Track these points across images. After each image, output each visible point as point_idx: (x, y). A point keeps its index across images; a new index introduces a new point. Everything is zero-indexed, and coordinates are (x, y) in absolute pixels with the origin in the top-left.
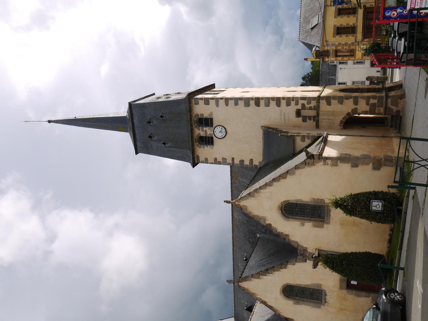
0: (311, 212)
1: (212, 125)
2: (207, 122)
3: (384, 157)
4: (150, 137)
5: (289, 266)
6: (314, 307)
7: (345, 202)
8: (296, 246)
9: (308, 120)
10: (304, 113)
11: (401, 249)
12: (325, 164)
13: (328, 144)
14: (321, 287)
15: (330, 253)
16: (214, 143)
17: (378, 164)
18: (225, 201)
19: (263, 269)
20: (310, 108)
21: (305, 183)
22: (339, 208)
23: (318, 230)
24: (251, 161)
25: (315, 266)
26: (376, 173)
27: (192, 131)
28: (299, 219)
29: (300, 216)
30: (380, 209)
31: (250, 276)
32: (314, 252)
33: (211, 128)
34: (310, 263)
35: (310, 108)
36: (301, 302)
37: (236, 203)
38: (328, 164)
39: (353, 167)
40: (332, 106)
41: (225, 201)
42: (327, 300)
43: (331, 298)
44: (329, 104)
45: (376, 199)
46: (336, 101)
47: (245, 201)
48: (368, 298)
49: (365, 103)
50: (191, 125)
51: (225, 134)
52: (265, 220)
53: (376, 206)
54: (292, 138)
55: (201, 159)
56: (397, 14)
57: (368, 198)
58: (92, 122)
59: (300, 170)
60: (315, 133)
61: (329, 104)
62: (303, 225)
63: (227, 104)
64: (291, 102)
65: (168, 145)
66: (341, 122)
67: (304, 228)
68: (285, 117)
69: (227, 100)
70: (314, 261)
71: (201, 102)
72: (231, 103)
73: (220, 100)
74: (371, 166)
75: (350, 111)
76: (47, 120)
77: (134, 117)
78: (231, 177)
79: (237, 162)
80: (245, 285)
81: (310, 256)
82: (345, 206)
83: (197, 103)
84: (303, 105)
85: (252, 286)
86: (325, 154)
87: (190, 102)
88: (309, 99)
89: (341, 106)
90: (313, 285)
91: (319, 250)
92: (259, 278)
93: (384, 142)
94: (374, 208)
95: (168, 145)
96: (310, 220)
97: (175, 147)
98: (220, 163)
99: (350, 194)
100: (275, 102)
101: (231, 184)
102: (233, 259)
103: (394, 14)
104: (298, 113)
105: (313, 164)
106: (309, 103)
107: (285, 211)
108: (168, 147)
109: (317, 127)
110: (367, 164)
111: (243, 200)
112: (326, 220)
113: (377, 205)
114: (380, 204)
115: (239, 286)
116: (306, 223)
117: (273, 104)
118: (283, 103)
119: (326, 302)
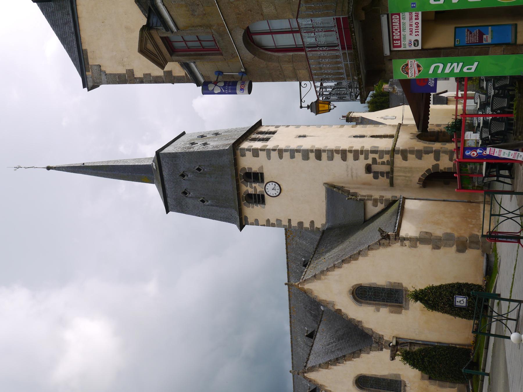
0: (389, 296)
1: (262, 181)
2: (257, 177)
3: (469, 237)
4: (185, 193)
5: (363, 355)
7: (425, 296)
8: (370, 333)
9: (380, 176)
10: (375, 168)
11: (487, 348)
12: (402, 245)
13: (406, 215)
14: (400, 377)
15: (410, 341)
16: (266, 201)
17: (462, 246)
19: (333, 357)
20: (383, 163)
21: (380, 267)
22: (419, 302)
24: (312, 223)
25: (393, 358)
26: (461, 256)
27: (238, 188)
29: (375, 301)
30: (464, 305)
31: (318, 366)
32: (391, 340)
33: (261, 184)
34: (386, 353)
35: (383, 163)
37: (300, 286)
38: (406, 246)
39: (434, 249)
43: (411, 389)
44: (405, 158)
45: (460, 294)
46: (414, 156)
47: (310, 284)
48: (454, 389)
49: (448, 158)
50: (237, 181)
51: (279, 191)
52: (334, 305)
53: (460, 302)
54: (363, 202)
55: (250, 220)
56: (477, 154)
57: (451, 292)
58: (107, 171)
59: (374, 251)
60: (389, 195)
61: (405, 158)
62: (378, 311)
63: (281, 157)
64: (360, 155)
65: (208, 203)
66: (420, 180)
67: (379, 314)
68: (352, 172)
69: (281, 152)
70: (392, 351)
71: (249, 154)
72: (286, 155)
73: (272, 153)
74: (454, 248)
76: (46, 166)
77: (163, 169)
78: (286, 236)
79: (294, 224)
80: (311, 375)
81: (387, 345)
82: (425, 300)
83: (244, 155)
84: (374, 160)
86: (402, 234)
87: (235, 154)
88: (382, 153)
90: (391, 375)
91: (397, 338)
92: (327, 368)
93: (470, 210)
94: (458, 304)
95: (208, 203)
96: (386, 306)
97: (217, 206)
98: (273, 225)
99: (431, 285)
100: (340, 155)
101: (286, 244)
103: (473, 154)
104: (368, 169)
105: (389, 245)
106: (381, 157)
107: (356, 294)
108: (208, 205)
109: (392, 184)
110: (451, 246)
113: (461, 301)
114: (465, 300)
115: (305, 378)
116: (381, 309)
117: (337, 157)
118: (350, 156)
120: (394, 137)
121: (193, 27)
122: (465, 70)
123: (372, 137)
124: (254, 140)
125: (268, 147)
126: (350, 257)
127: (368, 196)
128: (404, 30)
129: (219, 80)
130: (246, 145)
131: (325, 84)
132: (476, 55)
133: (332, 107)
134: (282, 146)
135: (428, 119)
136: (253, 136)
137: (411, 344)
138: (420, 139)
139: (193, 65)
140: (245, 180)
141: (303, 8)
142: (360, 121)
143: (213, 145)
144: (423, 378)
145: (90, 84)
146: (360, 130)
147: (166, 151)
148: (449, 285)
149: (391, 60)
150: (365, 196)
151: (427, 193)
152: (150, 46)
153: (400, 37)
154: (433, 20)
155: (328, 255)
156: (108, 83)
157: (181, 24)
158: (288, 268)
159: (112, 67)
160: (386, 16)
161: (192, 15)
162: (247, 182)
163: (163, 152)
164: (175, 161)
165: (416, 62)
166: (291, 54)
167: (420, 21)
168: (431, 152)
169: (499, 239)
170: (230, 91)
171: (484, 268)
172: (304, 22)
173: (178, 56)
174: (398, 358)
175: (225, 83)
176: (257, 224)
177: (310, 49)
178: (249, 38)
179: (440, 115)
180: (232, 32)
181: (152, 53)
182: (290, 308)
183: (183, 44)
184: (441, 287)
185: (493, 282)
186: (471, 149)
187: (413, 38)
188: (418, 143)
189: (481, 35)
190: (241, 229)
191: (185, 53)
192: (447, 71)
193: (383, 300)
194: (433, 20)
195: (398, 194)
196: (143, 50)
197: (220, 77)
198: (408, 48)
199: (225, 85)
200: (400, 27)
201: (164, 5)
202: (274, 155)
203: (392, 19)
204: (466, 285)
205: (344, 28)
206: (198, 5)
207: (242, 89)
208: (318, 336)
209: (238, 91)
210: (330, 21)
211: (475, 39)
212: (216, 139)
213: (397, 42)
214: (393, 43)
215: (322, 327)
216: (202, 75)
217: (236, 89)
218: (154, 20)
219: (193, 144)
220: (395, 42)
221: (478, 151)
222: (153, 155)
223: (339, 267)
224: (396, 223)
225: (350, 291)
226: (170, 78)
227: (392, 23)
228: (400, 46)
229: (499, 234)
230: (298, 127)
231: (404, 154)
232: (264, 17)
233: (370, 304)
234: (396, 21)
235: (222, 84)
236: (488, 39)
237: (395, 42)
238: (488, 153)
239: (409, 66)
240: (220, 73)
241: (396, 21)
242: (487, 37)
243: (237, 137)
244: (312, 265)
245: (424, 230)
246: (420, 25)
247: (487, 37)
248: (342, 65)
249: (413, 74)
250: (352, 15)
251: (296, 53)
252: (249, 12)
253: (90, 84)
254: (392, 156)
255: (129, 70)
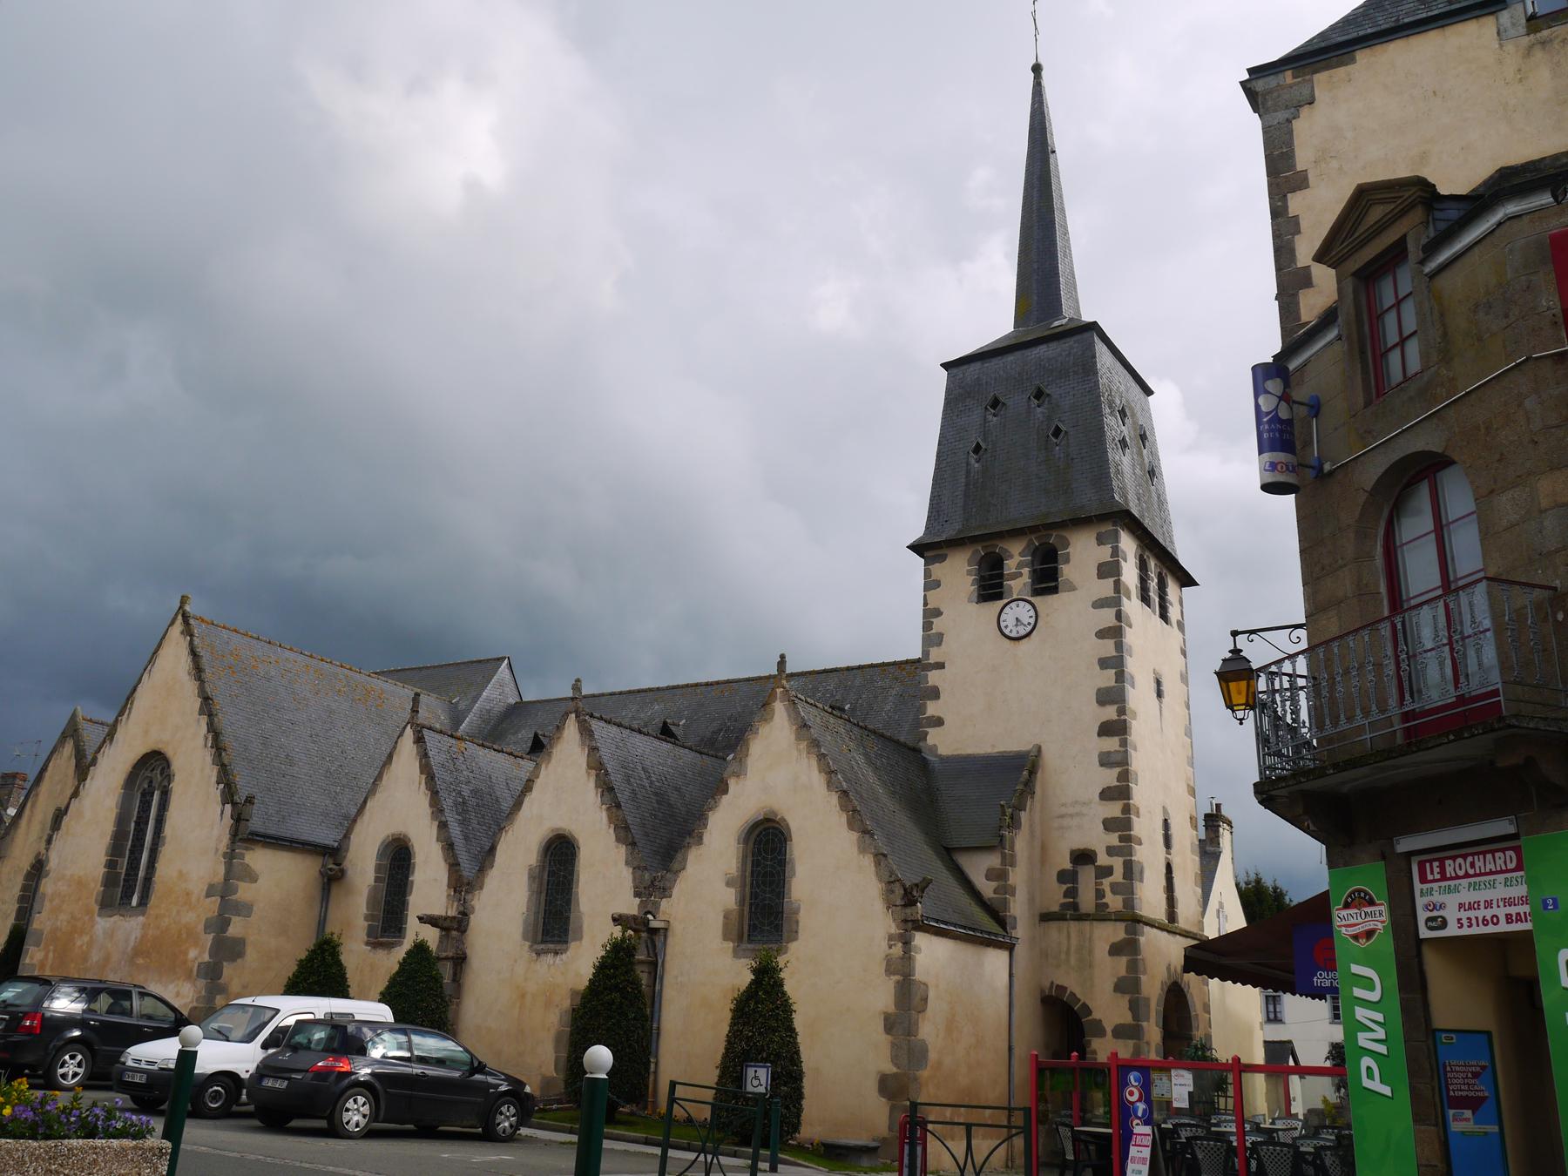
0: (764, 909)
1: (1037, 592)
2: (1047, 580)
4: (995, 403)
5: (623, 849)
6: (525, 922)
7: (766, 992)
8: (676, 866)
9: (1065, 887)
10: (1087, 875)
12: (891, 938)
14: (575, 940)
17: (890, 1087)
18: (782, 656)
19: (616, 778)
20: (1100, 894)
21: (838, 883)
23: (716, 924)
24: (939, 722)
25: (617, 920)
26: (872, 1085)
28: (744, 871)
30: (750, 1088)
32: (661, 916)
33: (1029, 589)
36: (535, 886)
39: (886, 1019)
40: (1109, 958)
41: (782, 656)
42: (543, 957)
44: (1115, 950)
45: (775, 1078)
46: (1123, 972)
51: (1014, 635)
52: (737, 775)
53: (756, 1078)
54: (997, 843)
55: (937, 569)
57: (778, 1056)
60: (1018, 908)
61: (1115, 950)
62: (728, 884)
63: (1101, 634)
66: (1062, 989)
68: (1071, 816)
69: (1114, 634)
70: (634, 918)
71: (1104, 553)
74: (890, 1068)
75: (1096, 1015)
77: (1053, 345)
78: (901, 663)
79: (934, 678)
80: (571, 729)
83: (1100, 541)
84: (1108, 871)
85: (569, 752)
86: (921, 940)
87: (1102, 518)
88: (1127, 889)
89: (1109, 986)
90: (580, 919)
92: (589, 767)
94: (751, 1072)
96: (741, 902)
97: (967, 485)
98: (927, 626)
99: (794, 1007)
101: (884, 664)
102: (674, 687)
103: (1132, 1094)
104: (1083, 857)
105: (890, 905)
106: (1115, 888)
109: (1046, 917)
110: (895, 1060)
111: (787, 710)
112: (746, 946)
113: (758, 1079)
114: (762, 1090)
115: (567, 714)
117: (1110, 777)
119: (538, 954)
120: (1170, 923)
121: (1442, 315)
122: (1366, 1062)
123: (1169, 868)
124: (1143, 566)
125: (1124, 599)
126: (854, 811)
127: (1013, 856)
128: (1475, 887)
129: (1295, 406)
130: (1128, 544)
131: (1302, 695)
132: (1413, 1089)
133: (1240, 714)
134: (1131, 637)
135: (1223, 979)
136: (1152, 563)
137: (654, 964)
138: (1169, 991)
139: (1332, 334)
140: (1037, 548)
141: (1524, 599)
142: (1209, 848)
143: (1124, 464)
144: (574, 993)
145: (1260, 85)
146: (1186, 837)
147: (1100, 348)
148: (797, 1052)
149: (1384, 857)
150: (1012, 848)
151: (1028, 1008)
152: (1376, 213)
153: (1452, 878)
154: (1510, 966)
155: (861, 760)
156: (1267, 131)
157: (1445, 282)
158: (825, 671)
159: (1308, 132)
160: (1512, 830)
161: (1477, 306)
162: (1033, 555)
163: (1096, 339)
164: (1075, 373)
165: (1380, 926)
166: (1383, 589)
167: (1503, 927)
168: (1136, 1016)
169: (907, 1148)
170: (1265, 436)
171: (843, 1141)
172: (1477, 606)
173: (1355, 292)
174: (617, 932)
175: (1289, 422)
176: (927, 588)
177: (1399, 626)
178: (1423, 469)
179: (1235, 1013)
180: (1435, 420)
181: (1358, 222)
182: (728, 682)
183: (1389, 300)
184: (791, 1030)
185: (811, 1161)
186: (1146, 1088)
187: (1451, 914)
188: (1158, 985)
189: (1474, 1104)
190: (913, 547)
191: (1365, 309)
192: (1361, 1013)
193: (754, 895)
194: (1510, 966)
195: (1021, 931)
196: (1364, 196)
197: (1302, 411)
198: (1420, 902)
199: (1281, 421)
200: (1481, 874)
201: (1499, 224)
202: (1107, 617)
203: (1503, 850)
204: (798, 1095)
205: (1470, 714)
206: (1507, 316)
207: (1273, 466)
208: (666, 746)
209: (1267, 456)
210: (1485, 664)
211: (1458, 1088)
212: (1138, 471)
213: (1436, 870)
214: (1431, 861)
215: (688, 756)
216: (1305, 364)
217: (1272, 450)
218: (1453, 213)
219: (1123, 413)
220: (1436, 864)
221: (1141, 1107)
222: (1087, 317)
223: (829, 785)
224: (946, 923)
225: (773, 812)
226: (1290, 283)
227: (1493, 852)
228: (1423, 880)
229: (919, 1149)
230: (1184, 679)
231: (1127, 948)
232: (1484, 498)
233: (744, 863)
234: (1500, 862)
235: (1284, 414)
236: (1462, 1123)
237: (1436, 864)
238: (1137, 1130)
239: (1369, 909)
240: (1315, 408)
241: (1500, 862)
242: (1467, 1120)
243: (1147, 523)
244: (832, 720)
245: (931, 994)
246: (1491, 929)
247: (1467, 1120)
248: (1359, 720)
249: (1346, 922)
250: (1510, 726)
251: (1385, 602)
252: (1497, 456)
253: (1263, 86)
254: (1118, 917)
255: (1306, 178)
